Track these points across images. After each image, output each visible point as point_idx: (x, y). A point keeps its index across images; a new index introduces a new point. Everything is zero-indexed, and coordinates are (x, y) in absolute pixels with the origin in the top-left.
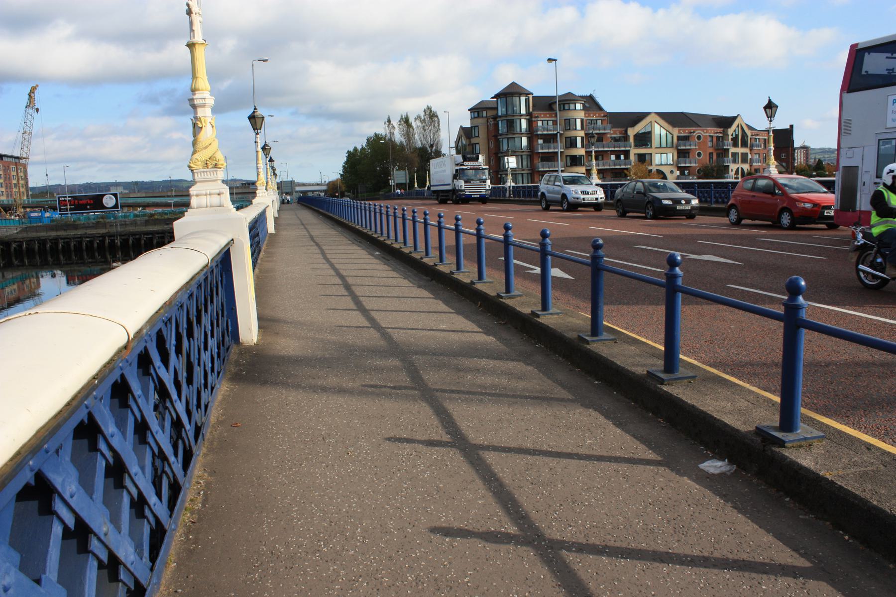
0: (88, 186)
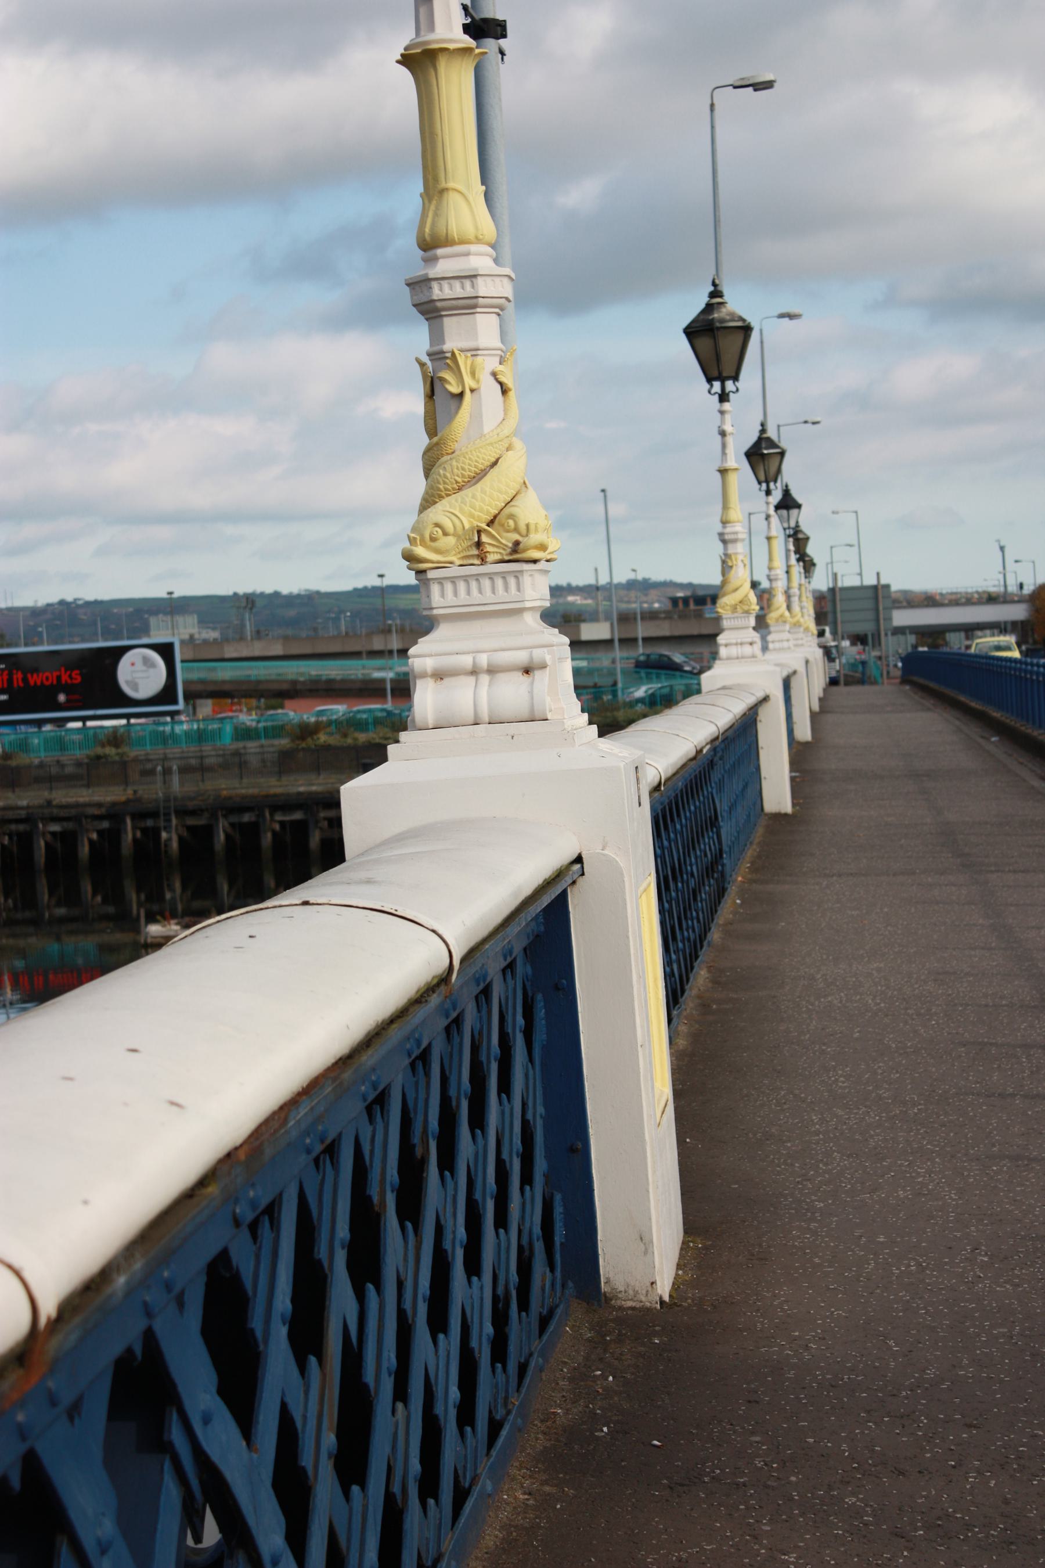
0: (65, 615)
